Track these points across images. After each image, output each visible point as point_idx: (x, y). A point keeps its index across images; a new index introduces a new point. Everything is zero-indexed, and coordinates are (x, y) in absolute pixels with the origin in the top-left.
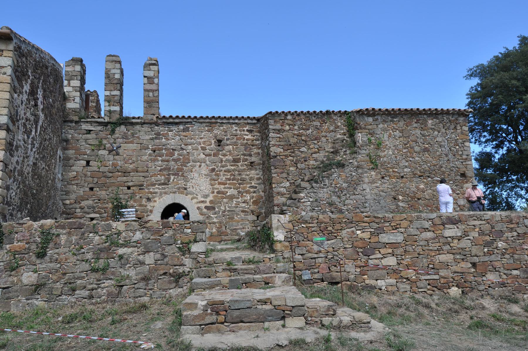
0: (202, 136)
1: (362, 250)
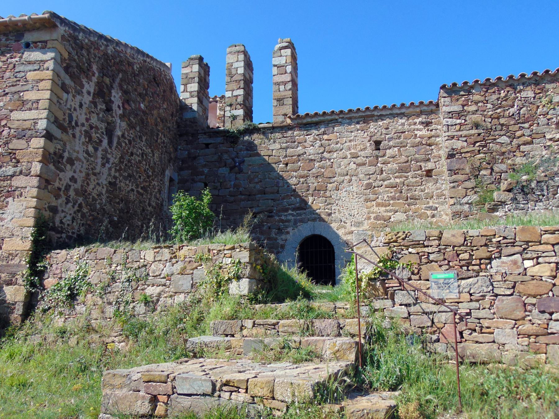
0: (352, 138)
1: (534, 301)
